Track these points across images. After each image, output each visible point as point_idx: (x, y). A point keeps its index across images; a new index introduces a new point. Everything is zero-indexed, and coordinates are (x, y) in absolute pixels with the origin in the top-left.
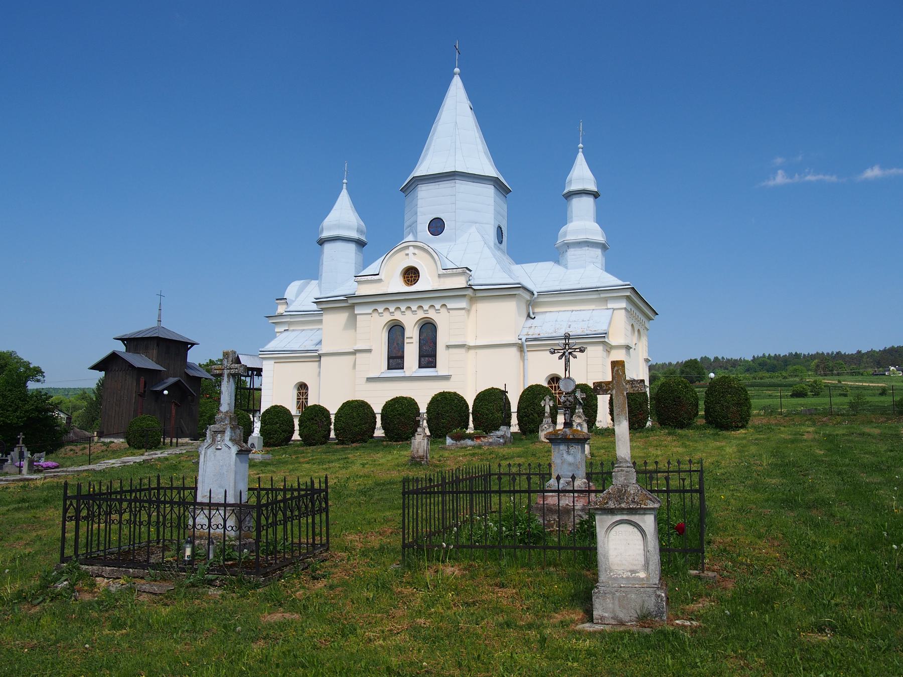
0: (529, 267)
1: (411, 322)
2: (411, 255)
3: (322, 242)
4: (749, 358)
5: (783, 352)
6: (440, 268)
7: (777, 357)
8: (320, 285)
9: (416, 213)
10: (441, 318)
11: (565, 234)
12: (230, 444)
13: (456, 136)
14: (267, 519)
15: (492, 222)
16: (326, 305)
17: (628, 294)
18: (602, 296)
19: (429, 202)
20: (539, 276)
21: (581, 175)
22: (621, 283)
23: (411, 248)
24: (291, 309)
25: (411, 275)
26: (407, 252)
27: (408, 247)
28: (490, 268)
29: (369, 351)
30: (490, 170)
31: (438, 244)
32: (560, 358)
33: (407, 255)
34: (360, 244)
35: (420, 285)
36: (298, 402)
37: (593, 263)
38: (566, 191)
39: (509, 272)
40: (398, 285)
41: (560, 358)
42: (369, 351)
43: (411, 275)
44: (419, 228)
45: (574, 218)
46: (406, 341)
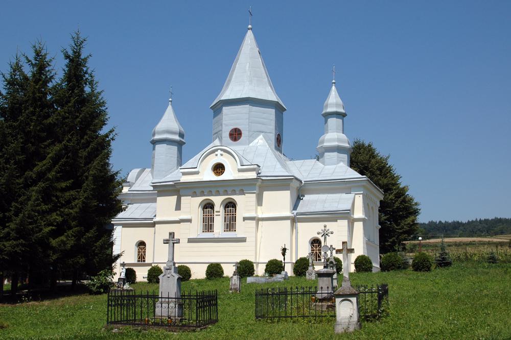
0: (298, 163)
1: (218, 200)
2: (219, 155)
3: (155, 142)
4: (491, 219)
5: (491, 217)
6: (239, 164)
7: (486, 221)
8: (152, 172)
9: (222, 125)
10: (237, 198)
11: (323, 142)
12: (174, 274)
13: (248, 76)
14: (199, 305)
15: (274, 132)
16: (162, 190)
17: (365, 184)
18: (347, 185)
19: (231, 117)
20: (305, 170)
21: (334, 102)
22: (361, 176)
23: (219, 151)
24: (133, 189)
25: (219, 168)
26: (216, 153)
27: (217, 150)
28: (273, 167)
29: (189, 221)
30: (272, 96)
31: (234, 147)
32: (328, 230)
33: (217, 155)
34: (180, 144)
35: (226, 176)
36: (138, 254)
37: (343, 161)
38: (324, 112)
39: (284, 166)
40: (208, 175)
41: (328, 230)
42: (189, 221)
43: (219, 168)
44: (224, 135)
45: (329, 131)
46: (215, 213)
